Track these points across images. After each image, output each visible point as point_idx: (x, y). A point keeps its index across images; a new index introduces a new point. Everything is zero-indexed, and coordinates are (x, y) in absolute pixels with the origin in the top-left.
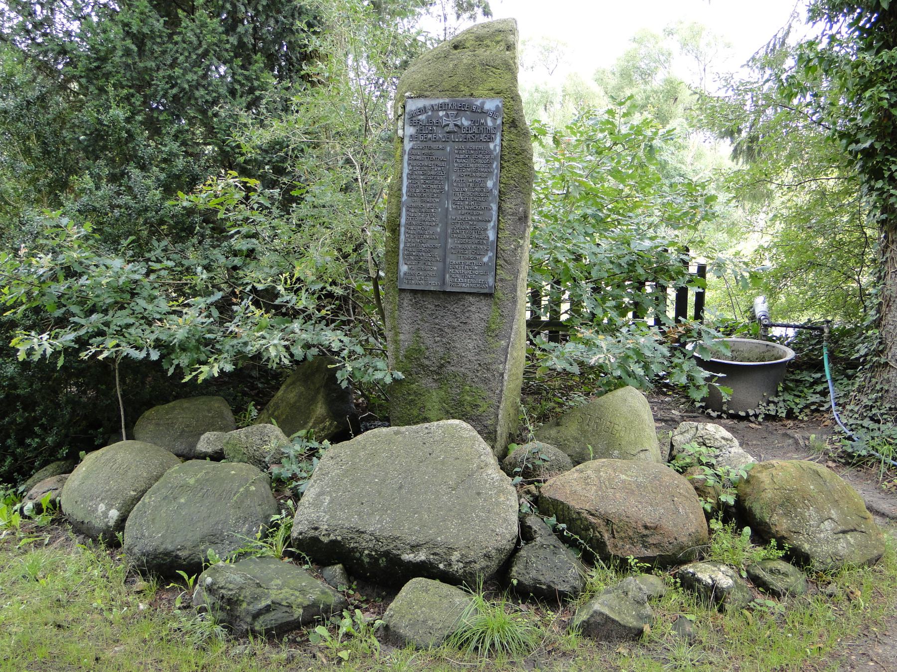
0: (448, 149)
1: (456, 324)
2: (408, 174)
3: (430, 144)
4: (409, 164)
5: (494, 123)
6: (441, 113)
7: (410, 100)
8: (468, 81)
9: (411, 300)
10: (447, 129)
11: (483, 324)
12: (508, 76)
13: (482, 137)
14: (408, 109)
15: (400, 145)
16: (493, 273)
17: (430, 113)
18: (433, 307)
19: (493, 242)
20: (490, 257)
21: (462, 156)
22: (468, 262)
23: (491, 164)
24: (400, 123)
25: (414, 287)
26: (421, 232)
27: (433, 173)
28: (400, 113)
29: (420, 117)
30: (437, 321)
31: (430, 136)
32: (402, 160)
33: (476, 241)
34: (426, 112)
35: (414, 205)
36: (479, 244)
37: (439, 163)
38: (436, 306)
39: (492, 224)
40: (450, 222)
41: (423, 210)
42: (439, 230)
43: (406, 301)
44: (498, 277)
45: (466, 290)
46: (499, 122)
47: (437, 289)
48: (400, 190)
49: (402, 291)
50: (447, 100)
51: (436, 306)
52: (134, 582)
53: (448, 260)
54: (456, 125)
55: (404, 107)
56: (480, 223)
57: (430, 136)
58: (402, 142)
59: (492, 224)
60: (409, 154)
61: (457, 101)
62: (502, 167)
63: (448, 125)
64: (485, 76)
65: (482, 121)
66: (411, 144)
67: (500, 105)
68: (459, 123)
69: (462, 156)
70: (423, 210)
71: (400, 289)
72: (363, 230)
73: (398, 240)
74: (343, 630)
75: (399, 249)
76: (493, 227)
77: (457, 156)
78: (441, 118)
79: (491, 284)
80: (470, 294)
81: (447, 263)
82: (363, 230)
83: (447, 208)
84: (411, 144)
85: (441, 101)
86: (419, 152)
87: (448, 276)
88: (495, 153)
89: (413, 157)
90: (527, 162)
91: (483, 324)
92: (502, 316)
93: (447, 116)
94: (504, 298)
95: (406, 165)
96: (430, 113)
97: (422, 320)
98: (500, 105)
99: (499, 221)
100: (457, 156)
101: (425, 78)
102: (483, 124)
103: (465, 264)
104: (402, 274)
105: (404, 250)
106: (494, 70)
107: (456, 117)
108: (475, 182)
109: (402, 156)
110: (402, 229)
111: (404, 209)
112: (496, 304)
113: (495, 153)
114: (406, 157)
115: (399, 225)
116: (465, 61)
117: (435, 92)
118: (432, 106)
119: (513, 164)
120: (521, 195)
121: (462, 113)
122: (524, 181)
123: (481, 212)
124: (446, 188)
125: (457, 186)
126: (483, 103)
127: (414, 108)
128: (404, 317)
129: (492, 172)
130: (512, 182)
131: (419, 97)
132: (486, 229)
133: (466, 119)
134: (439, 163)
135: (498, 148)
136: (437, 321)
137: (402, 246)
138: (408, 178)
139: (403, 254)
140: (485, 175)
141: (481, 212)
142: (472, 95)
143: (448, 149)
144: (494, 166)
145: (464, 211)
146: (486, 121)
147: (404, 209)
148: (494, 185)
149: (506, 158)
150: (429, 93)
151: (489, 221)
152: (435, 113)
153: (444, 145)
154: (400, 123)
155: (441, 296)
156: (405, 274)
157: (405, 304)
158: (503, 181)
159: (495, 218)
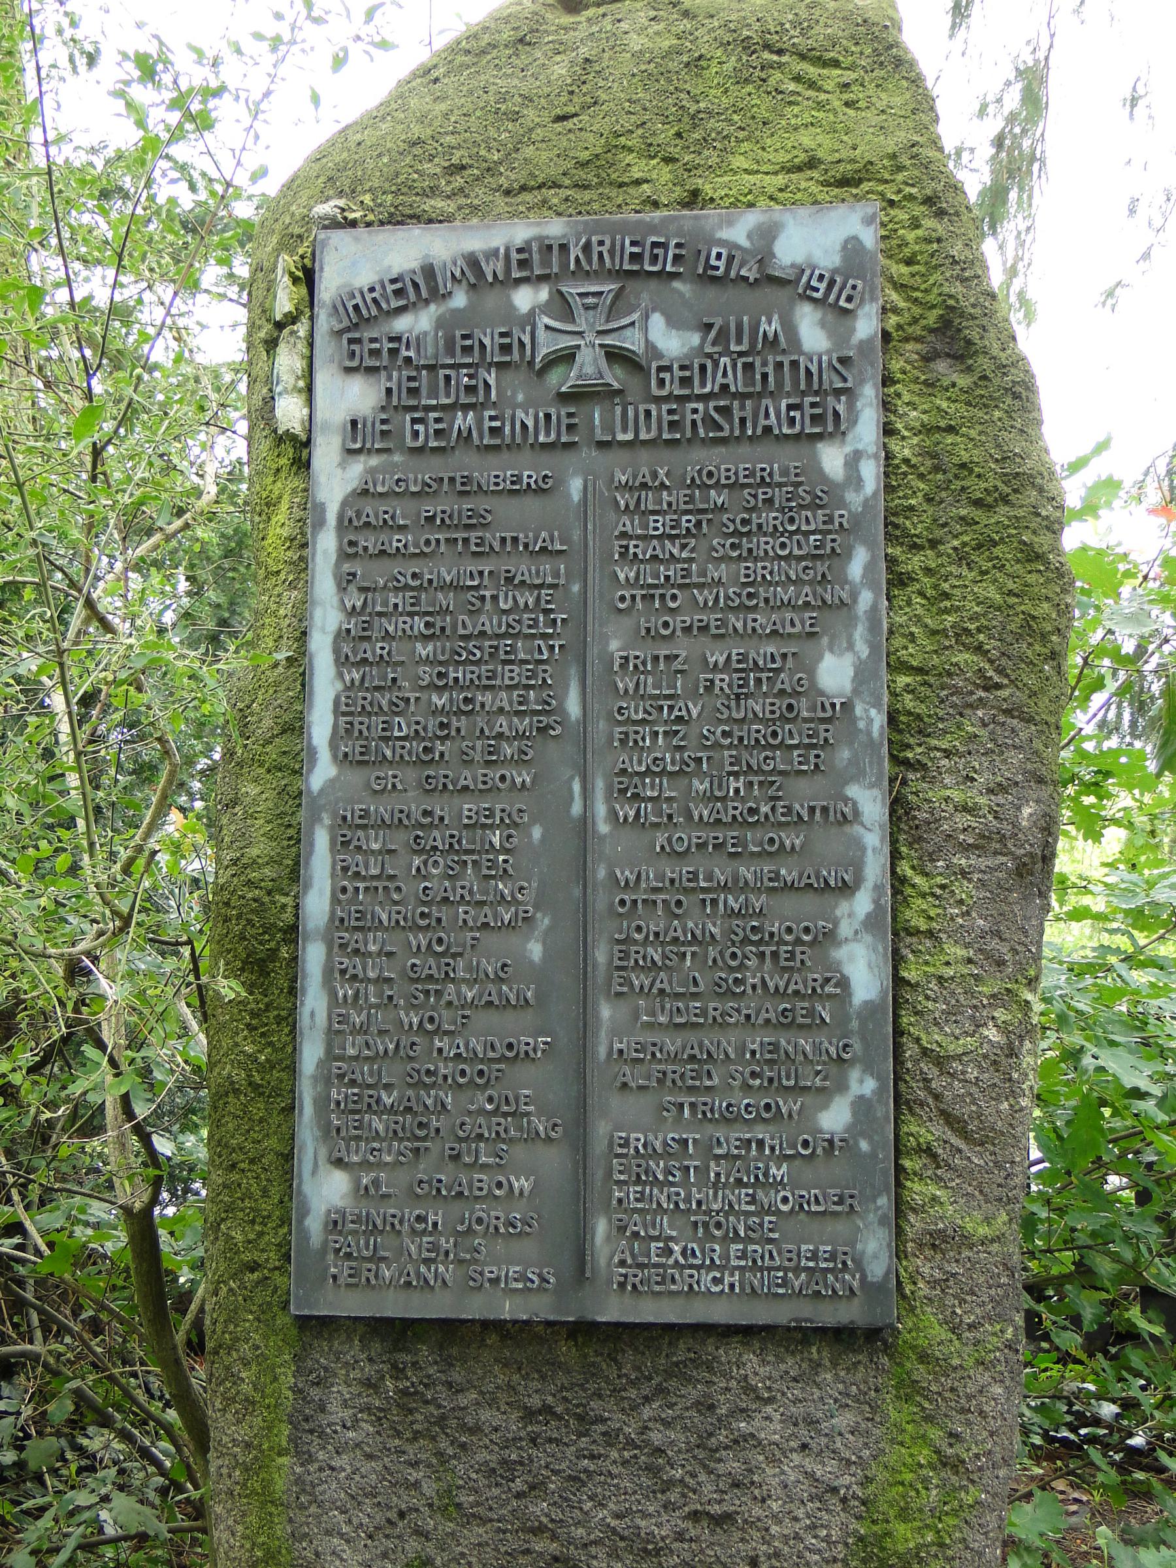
0: (575, 486)
1: (660, 1527)
2: (342, 635)
3: (466, 463)
4: (345, 581)
5: (840, 336)
6: (524, 299)
7: (339, 238)
8: (664, 134)
9: (370, 1385)
10: (562, 380)
11: (836, 1522)
12: (897, 99)
13: (774, 412)
14: (329, 286)
15: (286, 487)
16: (884, 1201)
17: (460, 300)
18: (514, 1425)
19: (871, 1008)
20: (861, 1106)
21: (659, 524)
22: (730, 1138)
23: (839, 556)
24: (288, 361)
25: (393, 1306)
26: (431, 966)
27: (488, 622)
28: (284, 303)
29: (402, 324)
30: (539, 1509)
31: (463, 421)
32: (302, 566)
33: (772, 1010)
34: (437, 295)
35: (381, 808)
36: (786, 1022)
37: (523, 569)
38: (529, 1415)
39: (862, 903)
40: (600, 901)
41: (438, 838)
42: (535, 950)
43: (340, 1390)
44: (915, 1224)
45: (720, 1313)
46: (866, 326)
47: (540, 1308)
48: (295, 727)
49: (321, 1327)
50: (555, 228)
51: (529, 1415)
52: (1094, 1234)
53: (601, 1129)
54: (614, 356)
55: (307, 277)
56: (789, 905)
57: (463, 421)
58: (302, 465)
59: (862, 903)
60: (343, 524)
61: (624, 228)
62: (898, 580)
63: (567, 357)
64: (762, 106)
65: (771, 326)
66: (357, 469)
67: (869, 238)
68: (632, 341)
69: (659, 524)
70: (438, 838)
71: (304, 1322)
72: (76, 971)
73: (290, 1020)
74: (447, 998)
75: (292, 1069)
76: (871, 923)
77: (628, 524)
78: (530, 319)
79: (877, 1269)
80: (746, 1333)
81: (599, 1147)
82: (76, 971)
83: (585, 823)
84: (357, 469)
85: (520, 232)
86: (401, 512)
87: (601, 1227)
88: (854, 500)
89: (369, 541)
90: (1042, 541)
91: (836, 1522)
92: (955, 1465)
93: (562, 306)
94: (958, 1353)
95: (324, 584)
96: (460, 300)
97: (447, 1506)
98: (869, 238)
99: (899, 883)
100: (628, 524)
101: (416, 131)
102: (772, 343)
103: (707, 1149)
104: (314, 1224)
105: (325, 1078)
106: (812, 71)
107: (612, 312)
108: (745, 667)
109: (301, 544)
110: (314, 956)
111: (322, 840)
112: (909, 1390)
113: (854, 500)
114: (327, 544)
115: (292, 932)
116: (636, 42)
117: (479, 195)
118: (473, 262)
119: (961, 557)
120: (1025, 732)
121: (645, 293)
122: (1033, 650)
123: (791, 839)
124: (573, 707)
125: (638, 694)
126: (767, 234)
127: (364, 278)
128: (331, 1490)
129: (845, 606)
130: (963, 658)
131: (396, 219)
132: (829, 937)
133: (673, 322)
134: (523, 569)
135: (870, 473)
136: (539, 1509)
137: (311, 1054)
138: (342, 662)
139: (322, 1104)
140: (801, 622)
141: (791, 839)
142: (693, 199)
143: (575, 486)
144: (856, 568)
145: (686, 837)
146: (790, 328)
147: (322, 840)
148: (861, 676)
149: (916, 527)
150: (450, 206)
151: (846, 889)
152: (491, 300)
153: (548, 464)
154: (288, 361)
155: (565, 1350)
156: (334, 1225)
157: (338, 1413)
158: (911, 654)
159: (875, 868)
